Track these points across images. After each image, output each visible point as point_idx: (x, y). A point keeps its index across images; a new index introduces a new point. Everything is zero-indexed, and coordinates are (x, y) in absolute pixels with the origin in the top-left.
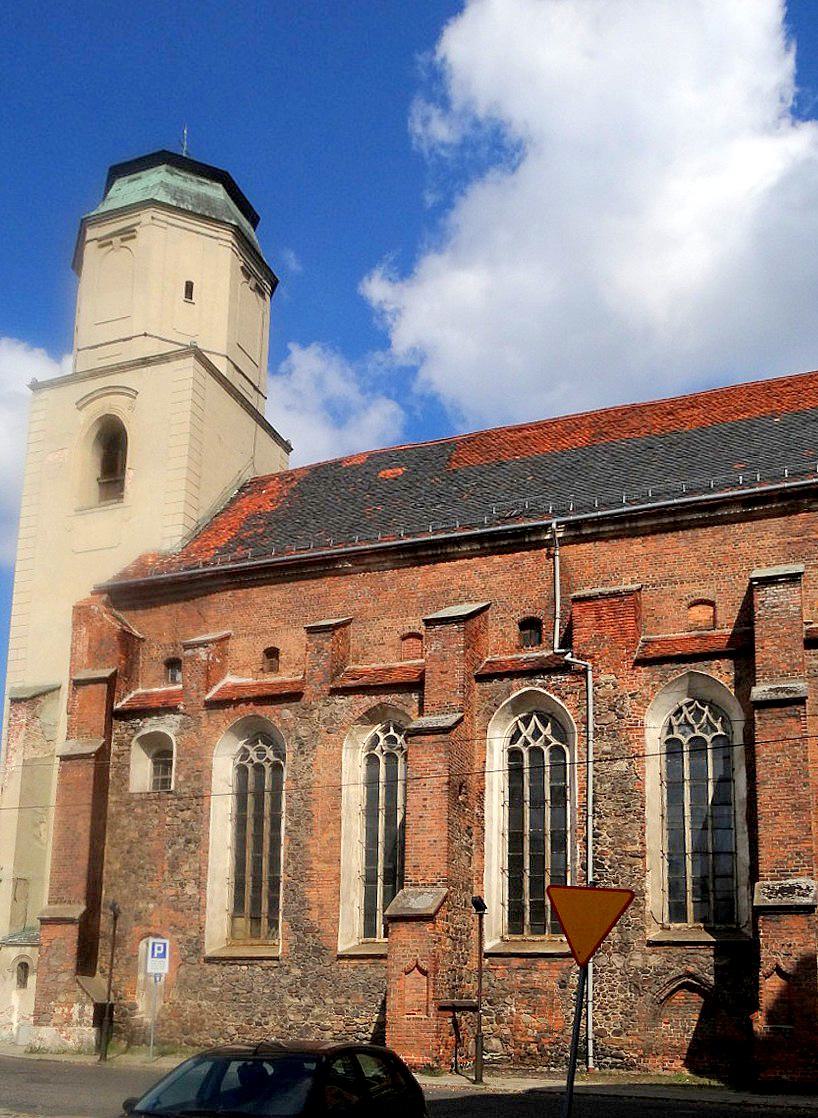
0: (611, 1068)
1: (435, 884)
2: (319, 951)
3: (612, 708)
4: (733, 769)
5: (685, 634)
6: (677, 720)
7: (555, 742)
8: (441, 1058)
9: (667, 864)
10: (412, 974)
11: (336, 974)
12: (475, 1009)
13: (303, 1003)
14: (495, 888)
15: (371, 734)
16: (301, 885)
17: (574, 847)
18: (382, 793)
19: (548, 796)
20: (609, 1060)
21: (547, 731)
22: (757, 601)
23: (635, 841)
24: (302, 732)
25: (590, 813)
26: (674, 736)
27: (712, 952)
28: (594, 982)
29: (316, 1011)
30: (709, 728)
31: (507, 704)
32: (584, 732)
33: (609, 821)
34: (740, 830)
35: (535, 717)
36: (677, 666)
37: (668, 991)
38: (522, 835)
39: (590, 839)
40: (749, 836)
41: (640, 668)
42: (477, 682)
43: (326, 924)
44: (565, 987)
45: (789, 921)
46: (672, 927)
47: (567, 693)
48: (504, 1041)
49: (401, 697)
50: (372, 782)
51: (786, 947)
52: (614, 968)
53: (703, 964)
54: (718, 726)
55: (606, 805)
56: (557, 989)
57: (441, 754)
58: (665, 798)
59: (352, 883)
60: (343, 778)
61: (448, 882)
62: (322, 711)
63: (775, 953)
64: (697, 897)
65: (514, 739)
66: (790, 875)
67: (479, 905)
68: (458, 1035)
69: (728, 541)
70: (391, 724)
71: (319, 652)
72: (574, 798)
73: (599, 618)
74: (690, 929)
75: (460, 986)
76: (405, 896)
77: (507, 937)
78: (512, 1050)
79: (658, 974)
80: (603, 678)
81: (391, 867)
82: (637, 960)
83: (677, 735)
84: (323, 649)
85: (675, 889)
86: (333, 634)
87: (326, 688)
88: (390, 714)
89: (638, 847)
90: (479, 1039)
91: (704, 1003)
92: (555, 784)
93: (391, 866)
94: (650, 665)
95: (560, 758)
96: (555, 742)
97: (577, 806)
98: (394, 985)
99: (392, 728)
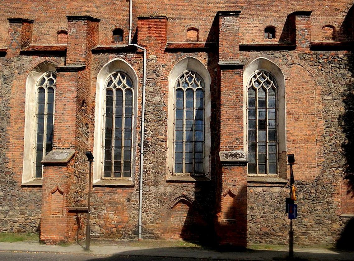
0: (149, 238)
1: (69, 149)
2: (13, 183)
3: (154, 71)
4: (205, 104)
5: (186, 43)
6: (182, 80)
7: (128, 87)
8: (69, 237)
9: (175, 146)
10: (55, 194)
11: (21, 195)
12: (86, 212)
13: (4, 209)
14: (99, 153)
15: (41, 77)
16: (4, 150)
17: (135, 136)
18: (46, 107)
19: (124, 112)
20: (148, 235)
21: (124, 82)
22: (221, 23)
23: (163, 134)
24: (6, 72)
25: (143, 119)
26: (180, 87)
27: (194, 186)
28: (142, 199)
29: (10, 213)
30: (195, 85)
31: (106, 66)
32: (141, 82)
33: (151, 124)
34: (206, 131)
35: (119, 74)
36: (184, 54)
37: (174, 203)
38: (111, 130)
39: (143, 132)
40: (211, 133)
41: (167, 53)
42: (93, 53)
43: (16, 170)
44: (129, 201)
45: (236, 169)
46: (176, 174)
47: (134, 63)
48: (101, 227)
49: (56, 58)
50: (41, 101)
51: (234, 181)
52: (151, 193)
53: (190, 191)
54: (199, 84)
55: (150, 117)
56: (126, 202)
57: (74, 82)
58: (175, 116)
59: (30, 150)
60: (26, 97)
61: (75, 148)
62: (16, 63)
63: (229, 184)
64: (187, 161)
65: (109, 84)
66: (234, 149)
67: (90, 156)
68: (79, 224)
69: (205, 3)
70: (51, 73)
71: (15, 33)
72: (136, 113)
73: (150, 28)
74: (184, 176)
75: (81, 201)
76: (53, 154)
77: (104, 178)
78: (104, 231)
79: (170, 196)
80: (151, 57)
81: (47, 141)
82: (162, 189)
83: (181, 87)
84: (17, 31)
85: (178, 158)
86: (23, 24)
87: (18, 51)
88: (50, 67)
89: (163, 137)
90: (88, 227)
91: (189, 209)
92: (127, 107)
93: (50, 143)
94: (172, 53)
95: (129, 95)
96: (128, 87)
97: (137, 117)
98: (46, 199)
99: (51, 75)
